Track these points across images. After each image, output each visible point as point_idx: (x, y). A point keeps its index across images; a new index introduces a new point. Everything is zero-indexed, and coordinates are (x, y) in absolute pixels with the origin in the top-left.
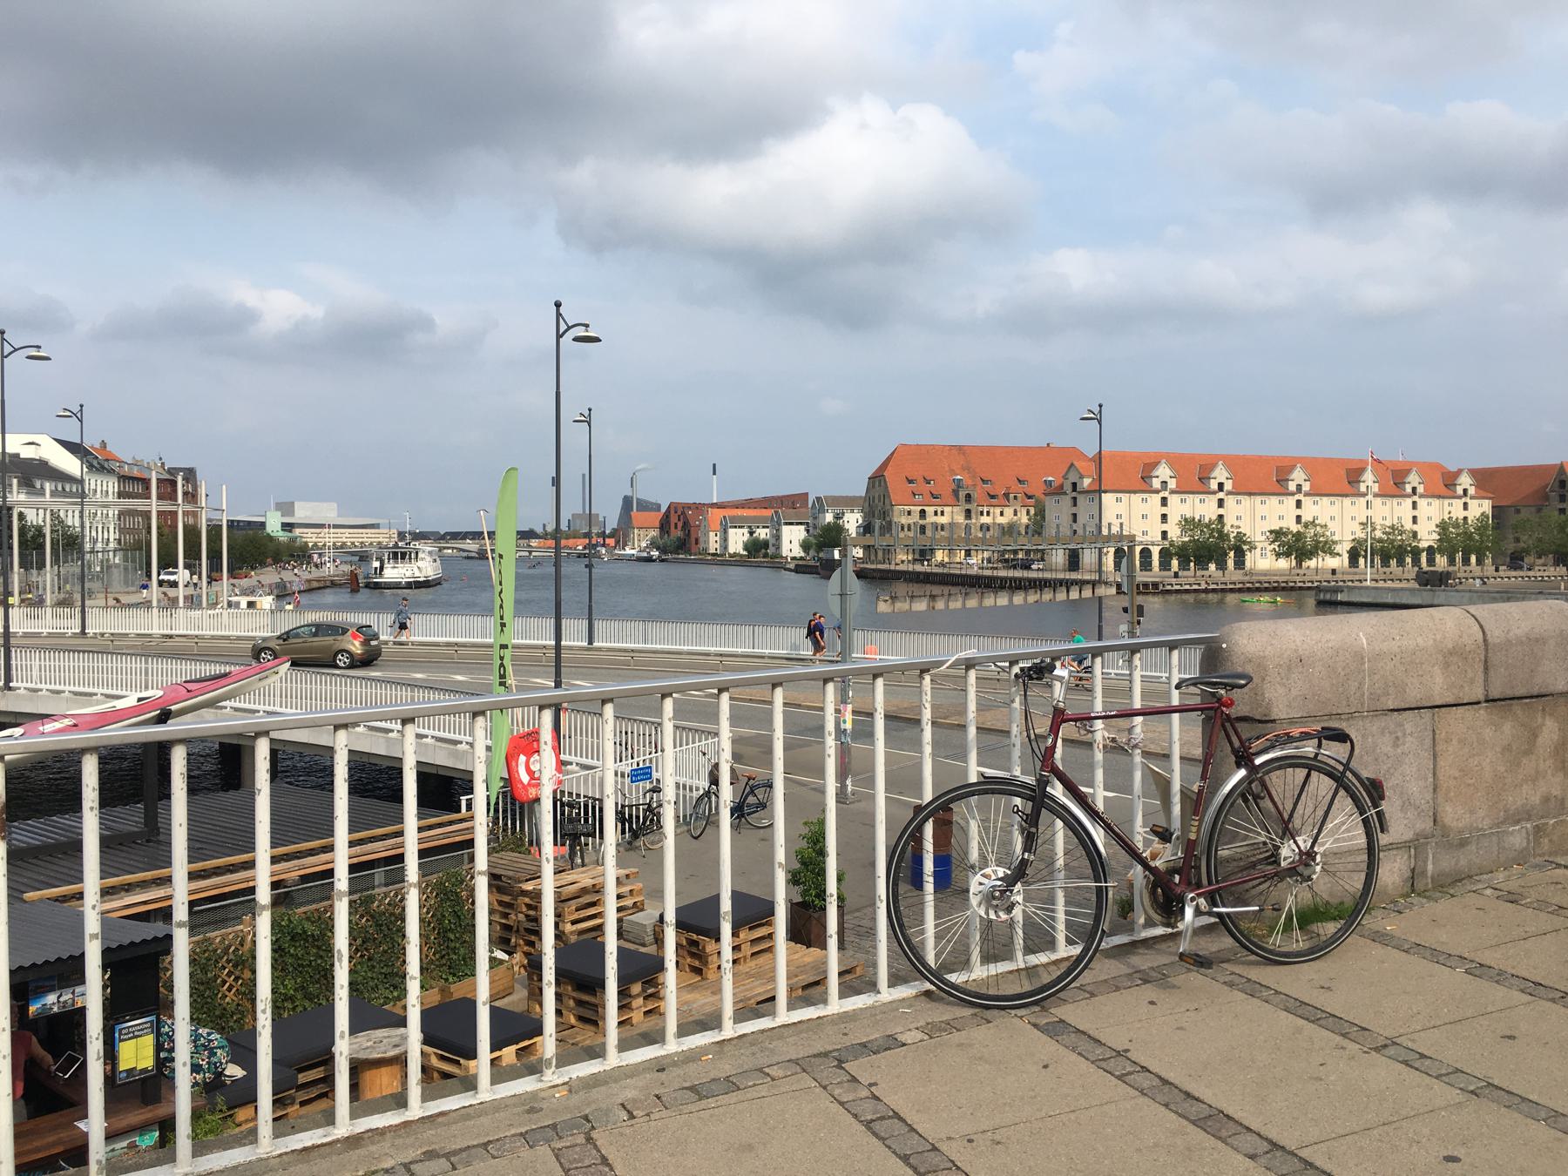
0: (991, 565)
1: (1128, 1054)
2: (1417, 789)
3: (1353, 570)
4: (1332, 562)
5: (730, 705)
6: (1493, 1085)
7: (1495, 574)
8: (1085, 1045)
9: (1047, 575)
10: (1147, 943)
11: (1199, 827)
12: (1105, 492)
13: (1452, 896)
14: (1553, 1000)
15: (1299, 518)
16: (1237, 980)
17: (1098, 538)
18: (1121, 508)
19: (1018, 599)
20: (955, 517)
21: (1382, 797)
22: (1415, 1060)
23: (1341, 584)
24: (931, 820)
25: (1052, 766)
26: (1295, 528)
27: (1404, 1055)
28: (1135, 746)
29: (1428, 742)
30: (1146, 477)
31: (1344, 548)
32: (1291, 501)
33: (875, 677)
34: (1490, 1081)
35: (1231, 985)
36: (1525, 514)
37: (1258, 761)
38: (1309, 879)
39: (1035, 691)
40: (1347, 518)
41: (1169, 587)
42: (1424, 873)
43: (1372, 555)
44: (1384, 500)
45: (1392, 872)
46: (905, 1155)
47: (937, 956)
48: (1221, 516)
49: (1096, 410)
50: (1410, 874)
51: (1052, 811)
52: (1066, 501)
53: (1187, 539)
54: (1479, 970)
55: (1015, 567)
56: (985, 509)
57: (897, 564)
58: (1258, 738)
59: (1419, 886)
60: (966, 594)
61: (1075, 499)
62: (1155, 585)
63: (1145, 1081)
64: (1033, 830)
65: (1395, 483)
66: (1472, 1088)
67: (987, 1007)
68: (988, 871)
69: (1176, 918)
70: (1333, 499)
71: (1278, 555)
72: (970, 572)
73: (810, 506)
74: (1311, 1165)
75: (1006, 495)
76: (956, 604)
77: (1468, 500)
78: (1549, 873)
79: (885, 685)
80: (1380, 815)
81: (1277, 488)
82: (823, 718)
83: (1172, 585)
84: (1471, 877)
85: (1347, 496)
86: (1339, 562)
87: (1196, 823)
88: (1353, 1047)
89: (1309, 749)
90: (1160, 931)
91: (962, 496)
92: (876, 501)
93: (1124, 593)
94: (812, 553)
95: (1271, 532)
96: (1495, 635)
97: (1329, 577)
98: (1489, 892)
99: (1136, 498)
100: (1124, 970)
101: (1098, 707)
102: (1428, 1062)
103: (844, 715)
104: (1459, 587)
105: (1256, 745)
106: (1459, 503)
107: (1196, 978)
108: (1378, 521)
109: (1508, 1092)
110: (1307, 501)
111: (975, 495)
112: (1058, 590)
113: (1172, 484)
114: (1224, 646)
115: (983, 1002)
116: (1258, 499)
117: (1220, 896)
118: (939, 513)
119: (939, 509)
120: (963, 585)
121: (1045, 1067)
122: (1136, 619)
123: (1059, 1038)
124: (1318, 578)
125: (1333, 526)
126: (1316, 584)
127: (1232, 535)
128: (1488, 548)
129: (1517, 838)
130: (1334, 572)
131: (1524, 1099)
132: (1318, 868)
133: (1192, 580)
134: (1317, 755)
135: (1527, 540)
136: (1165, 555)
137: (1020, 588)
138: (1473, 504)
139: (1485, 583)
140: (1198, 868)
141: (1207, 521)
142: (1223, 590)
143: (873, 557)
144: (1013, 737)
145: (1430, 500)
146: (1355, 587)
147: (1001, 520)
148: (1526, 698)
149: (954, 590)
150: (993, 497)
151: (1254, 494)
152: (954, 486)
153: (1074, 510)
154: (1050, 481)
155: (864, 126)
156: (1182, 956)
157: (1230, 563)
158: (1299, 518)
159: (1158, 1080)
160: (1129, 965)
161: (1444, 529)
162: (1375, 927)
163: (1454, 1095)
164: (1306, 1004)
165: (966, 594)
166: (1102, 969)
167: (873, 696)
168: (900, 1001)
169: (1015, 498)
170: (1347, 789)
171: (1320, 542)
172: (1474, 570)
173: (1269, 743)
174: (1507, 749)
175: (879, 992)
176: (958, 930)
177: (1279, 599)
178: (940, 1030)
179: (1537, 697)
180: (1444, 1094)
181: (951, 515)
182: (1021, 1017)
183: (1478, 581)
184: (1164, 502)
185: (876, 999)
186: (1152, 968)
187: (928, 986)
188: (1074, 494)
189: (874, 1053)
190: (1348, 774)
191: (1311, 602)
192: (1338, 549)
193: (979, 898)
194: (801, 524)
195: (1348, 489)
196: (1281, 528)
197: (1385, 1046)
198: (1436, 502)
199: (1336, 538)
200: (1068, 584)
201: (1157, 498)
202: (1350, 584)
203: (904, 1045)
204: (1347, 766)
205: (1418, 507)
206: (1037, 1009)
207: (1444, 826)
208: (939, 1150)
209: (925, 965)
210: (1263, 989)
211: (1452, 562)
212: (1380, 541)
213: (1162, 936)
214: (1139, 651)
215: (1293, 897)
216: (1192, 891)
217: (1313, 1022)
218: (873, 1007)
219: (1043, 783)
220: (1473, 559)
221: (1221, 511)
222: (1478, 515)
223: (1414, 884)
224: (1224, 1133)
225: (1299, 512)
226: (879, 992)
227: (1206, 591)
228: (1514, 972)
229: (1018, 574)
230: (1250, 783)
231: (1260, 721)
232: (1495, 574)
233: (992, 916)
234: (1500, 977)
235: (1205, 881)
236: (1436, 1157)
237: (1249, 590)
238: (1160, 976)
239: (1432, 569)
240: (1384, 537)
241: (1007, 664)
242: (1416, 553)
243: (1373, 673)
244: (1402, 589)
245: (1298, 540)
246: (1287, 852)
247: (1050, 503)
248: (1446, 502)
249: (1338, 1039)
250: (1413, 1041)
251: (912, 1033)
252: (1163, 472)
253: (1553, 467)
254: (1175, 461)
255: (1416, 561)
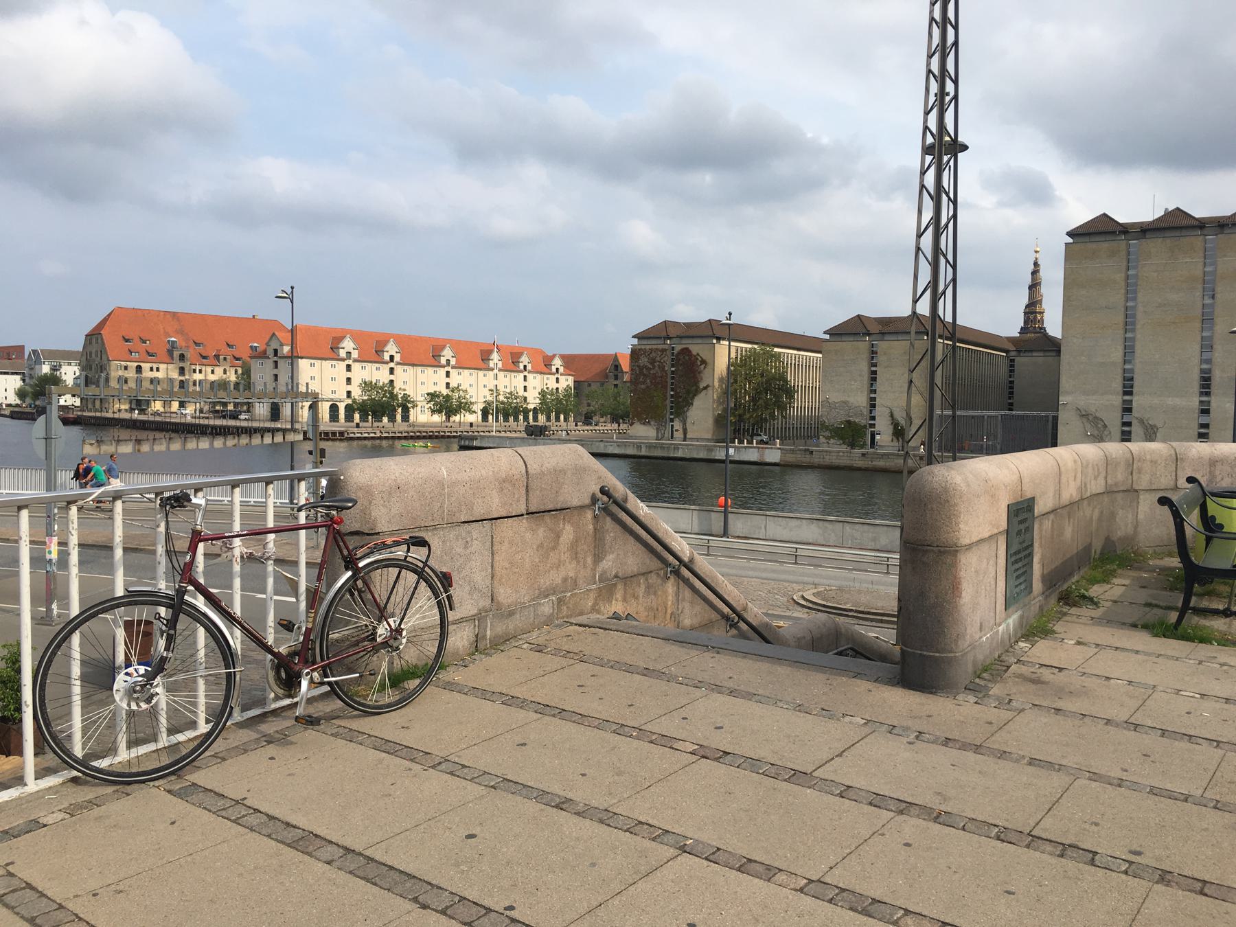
0: (202, 415)
1: (245, 802)
2: (481, 578)
3: (485, 424)
4: (470, 418)
5: (30, 548)
6: (506, 779)
7: (576, 428)
8: (209, 800)
9: (255, 424)
10: (274, 712)
11: (315, 618)
12: (302, 358)
13: (502, 651)
14: (554, 716)
15: (448, 384)
16: (341, 730)
17: (294, 394)
18: (314, 371)
19: (218, 443)
20: (170, 373)
21: (451, 585)
22: (457, 770)
23: (476, 434)
24: (77, 631)
25: (190, 578)
26: (445, 392)
27: (450, 767)
28: (268, 558)
29: (488, 544)
30: (335, 348)
31: (478, 407)
32: (442, 372)
33: (20, 508)
34: (505, 777)
35: (336, 735)
36: (594, 387)
37: (361, 565)
38: (398, 648)
39: (178, 516)
40: (481, 386)
41: (352, 435)
42: (484, 637)
43: (497, 413)
44: (506, 373)
45: (459, 639)
46: (32, 917)
47: (84, 745)
48: (392, 381)
49: (289, 291)
50: (474, 639)
51: (189, 614)
52: (269, 364)
53: (366, 398)
54: (511, 701)
55: (224, 417)
56: (198, 368)
57: (114, 413)
58: (362, 547)
59: (481, 646)
60: (170, 439)
61: (276, 362)
62: (341, 433)
63: (253, 820)
64: (172, 632)
65: (513, 362)
66: (492, 784)
67: (129, 783)
68: (130, 670)
69: (295, 690)
70: (471, 371)
71: (433, 412)
72: (183, 421)
73: (26, 357)
74: (372, 860)
75: (217, 357)
76: (160, 447)
77: (559, 376)
78: (564, 630)
79: (29, 516)
80: (449, 597)
81: (432, 361)
82: (17, 550)
83: (354, 433)
84: (516, 637)
85: (481, 369)
86: (475, 418)
87: (313, 615)
88: (417, 768)
89: (400, 553)
90: (287, 702)
91: (173, 354)
92: (93, 355)
93: (310, 439)
94: (28, 400)
95: (428, 394)
96: (534, 468)
97: (468, 428)
98: (525, 646)
99: (327, 364)
100: (255, 735)
101: (237, 527)
102: (466, 770)
103: (50, 547)
104: (552, 437)
105: (360, 553)
106: (553, 378)
107: (310, 734)
108: (501, 388)
109: (515, 783)
110: (453, 372)
111: (188, 355)
112: (254, 436)
113: (355, 355)
114: (342, 477)
115: (124, 779)
116: (419, 369)
117: (330, 670)
118: (155, 369)
119: (155, 366)
120: (167, 431)
121: (173, 823)
122: (319, 459)
123: (189, 799)
124: (461, 429)
125: (471, 391)
126: (459, 434)
127: (400, 396)
128: (571, 410)
129: (546, 608)
130: (471, 425)
131: (525, 786)
132: (404, 641)
133: (370, 430)
134: (406, 557)
135: (595, 405)
136: (350, 410)
137: (206, 434)
138: (562, 379)
139: (568, 434)
140: (313, 649)
141: (381, 384)
142: (393, 438)
143: (90, 406)
144: (158, 556)
145: (535, 375)
146: (485, 436)
147: (212, 378)
148: (536, 513)
149: (159, 435)
150: (204, 357)
151: (417, 365)
152: (168, 347)
153: (275, 371)
154: (256, 347)
155: (83, 22)
156: (297, 719)
157: (399, 417)
158: (448, 384)
159: (265, 817)
160: (258, 732)
161: (543, 396)
162: (447, 679)
163: (481, 790)
164: (389, 741)
165: (170, 439)
166: (234, 738)
167: (18, 527)
168: (46, 789)
169: (225, 359)
170: (426, 581)
171: (462, 403)
172: (562, 425)
173: (369, 550)
174: (540, 546)
175: (26, 785)
176: (102, 723)
177: (429, 444)
178: (82, 808)
179: (560, 510)
180: (474, 790)
181: (167, 372)
182: (158, 787)
183: (564, 433)
184: (349, 368)
185: (23, 791)
186: (277, 732)
187: (75, 773)
188: (275, 358)
189: (15, 837)
190: (427, 569)
191: (456, 446)
192: (475, 408)
193: (121, 694)
194: (17, 373)
195: (481, 364)
196: (435, 392)
197: (440, 763)
198: (539, 377)
199: (473, 400)
200: (273, 431)
201: (343, 365)
202: (482, 434)
203: (45, 826)
204: (425, 564)
205: (451, 376)
206: (173, 778)
207: (498, 602)
208: (65, 908)
209: (71, 755)
210: (360, 735)
211: (548, 419)
212: (502, 403)
213: (289, 705)
214: (272, 483)
215: (383, 664)
216: (307, 668)
217: (392, 754)
218: (19, 798)
219: (181, 592)
220: (562, 417)
221: (392, 377)
222: (565, 387)
223: (477, 647)
224: (311, 849)
225: (448, 380)
226: (26, 785)
227: (380, 438)
228: (533, 700)
229: (232, 423)
230: (355, 581)
231: (368, 534)
232: (576, 428)
233: (134, 707)
234: (522, 703)
235: (318, 659)
236: (461, 837)
237: (412, 438)
238: (282, 736)
239: (536, 424)
240: (505, 400)
241: (154, 496)
242: (526, 411)
243: (450, 496)
244: (516, 438)
245: (447, 401)
246: (382, 631)
247: (255, 366)
248: (546, 376)
249: (407, 763)
250: (459, 757)
251: (55, 815)
252: (348, 345)
253: (610, 355)
254: (358, 337)
255: (526, 418)
